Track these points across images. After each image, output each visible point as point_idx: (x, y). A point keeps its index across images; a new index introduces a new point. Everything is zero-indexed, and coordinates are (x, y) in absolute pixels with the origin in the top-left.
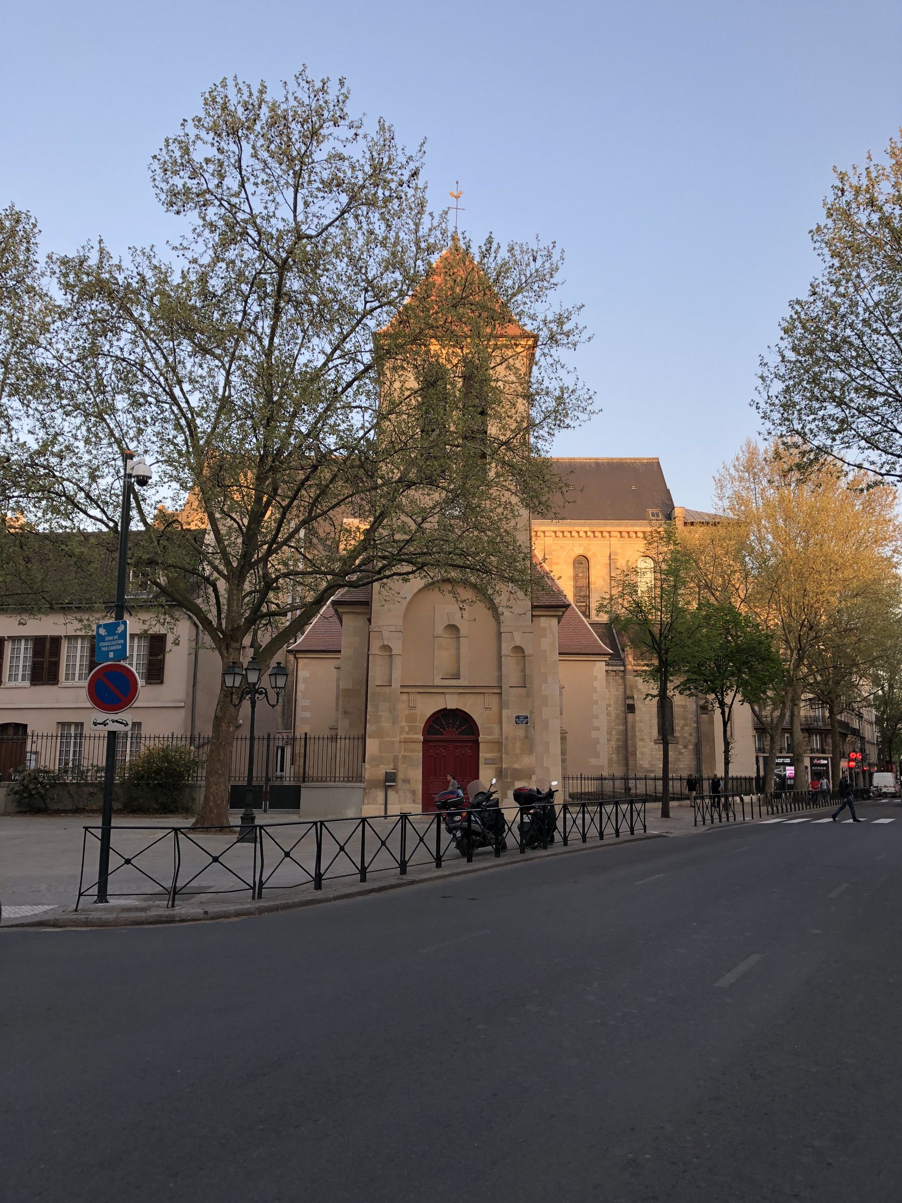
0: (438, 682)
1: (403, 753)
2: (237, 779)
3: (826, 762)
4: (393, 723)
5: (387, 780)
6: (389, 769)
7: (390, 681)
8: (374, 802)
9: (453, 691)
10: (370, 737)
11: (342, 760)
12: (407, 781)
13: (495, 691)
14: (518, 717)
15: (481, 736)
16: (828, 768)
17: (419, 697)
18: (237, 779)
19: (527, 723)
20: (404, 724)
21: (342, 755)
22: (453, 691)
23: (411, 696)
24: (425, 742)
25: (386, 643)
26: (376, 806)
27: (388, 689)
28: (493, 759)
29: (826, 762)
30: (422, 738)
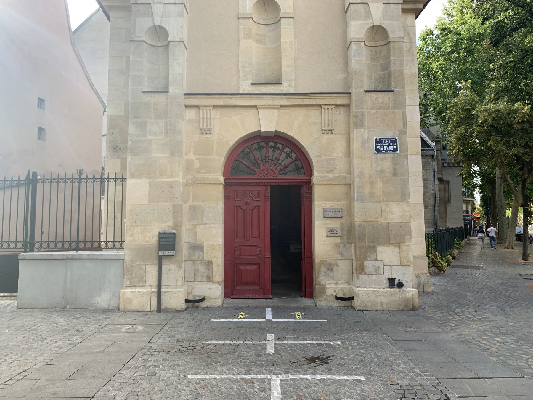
0: (246, 87)
1: (190, 203)
2: (12, 245)
3: (469, 218)
4: (172, 154)
5: (161, 247)
6: (167, 226)
7: (167, 87)
8: (141, 281)
9: (270, 102)
10: (133, 176)
11: (111, 215)
12: (197, 247)
13: (339, 101)
14: (379, 141)
15: (316, 174)
16: (470, 222)
17: (215, 114)
18: (12, 245)
19: (395, 150)
20: (192, 156)
21: (111, 208)
22: (270, 102)
23: (204, 112)
24: (228, 184)
25: (158, 22)
26: (144, 290)
27: (161, 98)
28: (336, 211)
29: (469, 218)
30: (222, 179)
